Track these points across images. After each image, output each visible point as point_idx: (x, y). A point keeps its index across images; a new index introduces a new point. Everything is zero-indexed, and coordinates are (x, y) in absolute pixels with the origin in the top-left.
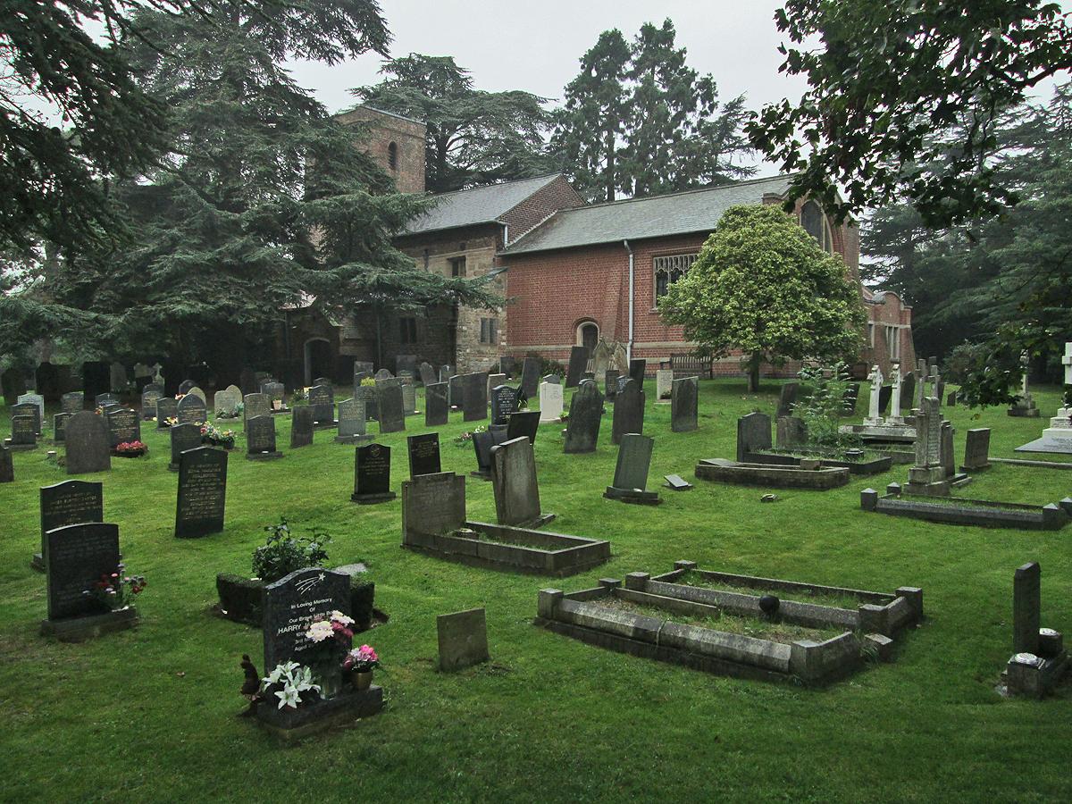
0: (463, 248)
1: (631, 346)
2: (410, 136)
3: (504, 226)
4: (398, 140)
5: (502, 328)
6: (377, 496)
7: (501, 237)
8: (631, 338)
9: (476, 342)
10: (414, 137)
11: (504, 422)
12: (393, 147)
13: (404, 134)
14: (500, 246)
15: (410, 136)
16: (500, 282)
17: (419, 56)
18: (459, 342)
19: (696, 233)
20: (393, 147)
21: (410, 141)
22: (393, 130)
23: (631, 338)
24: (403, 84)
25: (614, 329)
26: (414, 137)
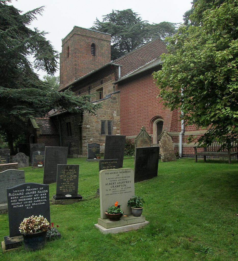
0: (102, 83)
1: (183, 134)
2: (102, 40)
3: (118, 67)
4: (96, 42)
5: (117, 125)
6: (157, 128)
7: (116, 74)
8: (182, 128)
9: (97, 134)
10: (105, 40)
11: (179, 113)
12: (93, 45)
13: (99, 39)
14: (117, 78)
15: (102, 40)
16: (115, 99)
17: (118, 11)
18: (84, 134)
19: (102, 206)
20: (93, 45)
21: (102, 42)
22: (93, 37)
23: (182, 128)
24: (169, 79)
25: (170, 122)
26: (105, 40)
